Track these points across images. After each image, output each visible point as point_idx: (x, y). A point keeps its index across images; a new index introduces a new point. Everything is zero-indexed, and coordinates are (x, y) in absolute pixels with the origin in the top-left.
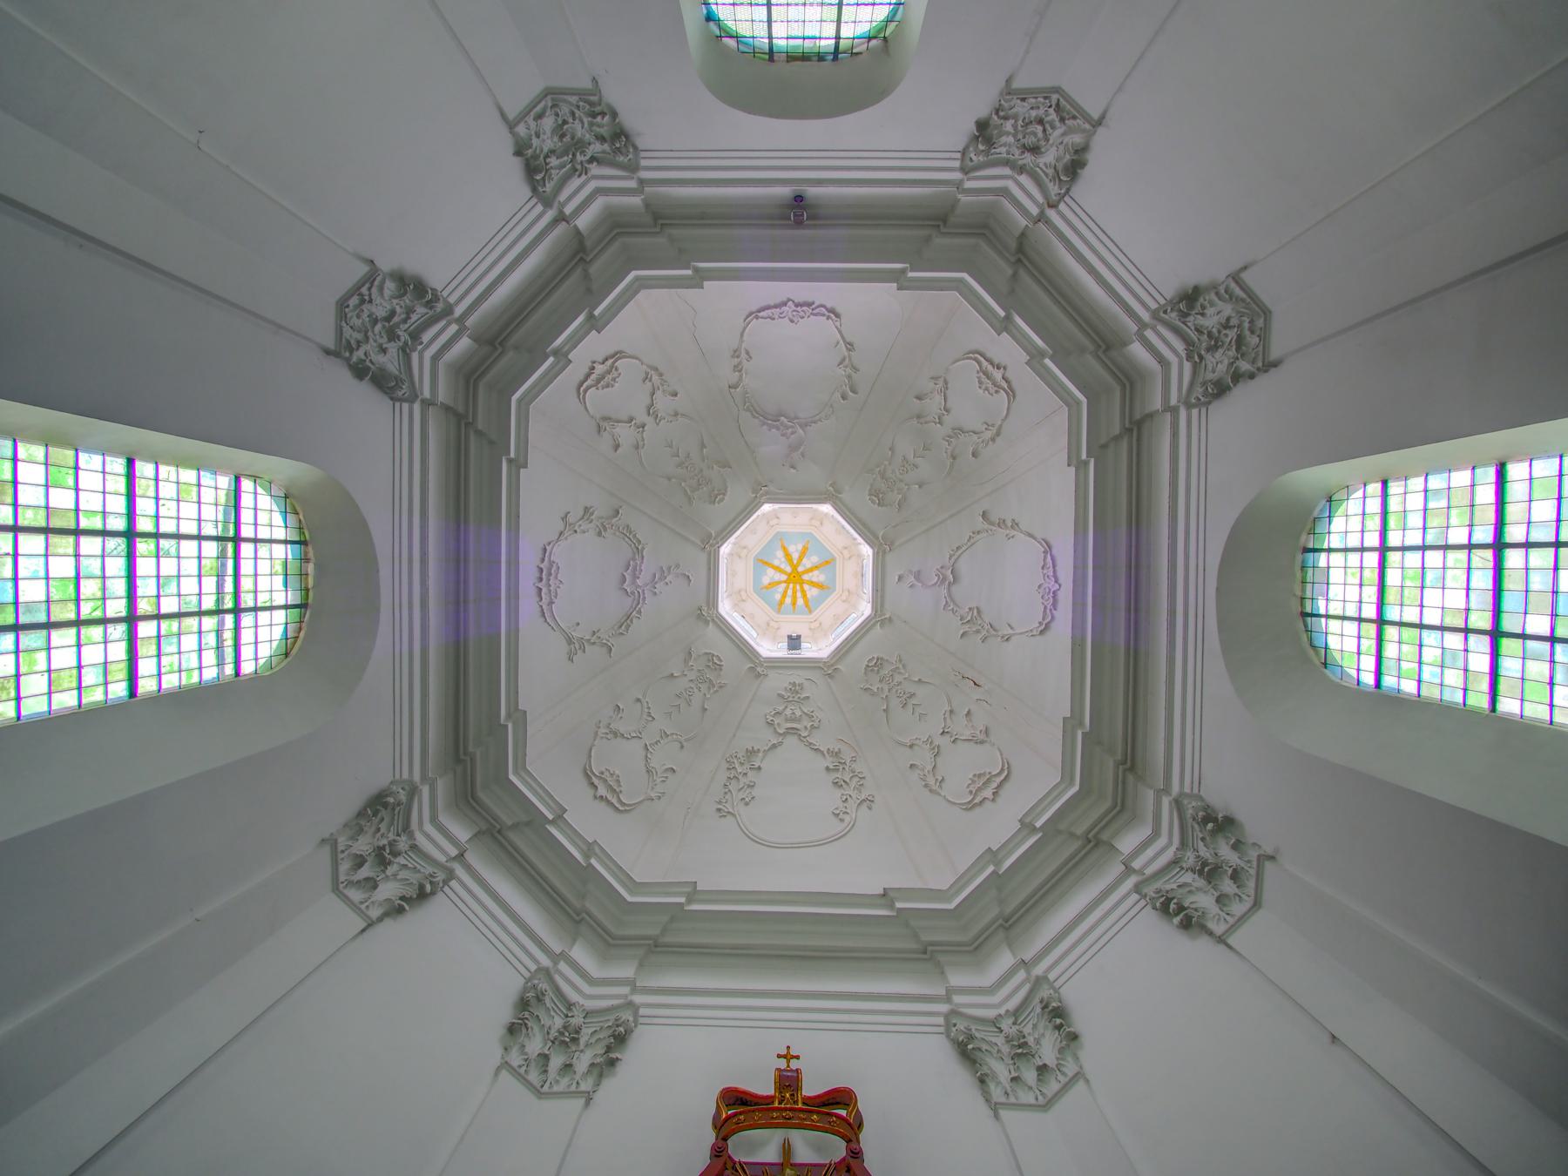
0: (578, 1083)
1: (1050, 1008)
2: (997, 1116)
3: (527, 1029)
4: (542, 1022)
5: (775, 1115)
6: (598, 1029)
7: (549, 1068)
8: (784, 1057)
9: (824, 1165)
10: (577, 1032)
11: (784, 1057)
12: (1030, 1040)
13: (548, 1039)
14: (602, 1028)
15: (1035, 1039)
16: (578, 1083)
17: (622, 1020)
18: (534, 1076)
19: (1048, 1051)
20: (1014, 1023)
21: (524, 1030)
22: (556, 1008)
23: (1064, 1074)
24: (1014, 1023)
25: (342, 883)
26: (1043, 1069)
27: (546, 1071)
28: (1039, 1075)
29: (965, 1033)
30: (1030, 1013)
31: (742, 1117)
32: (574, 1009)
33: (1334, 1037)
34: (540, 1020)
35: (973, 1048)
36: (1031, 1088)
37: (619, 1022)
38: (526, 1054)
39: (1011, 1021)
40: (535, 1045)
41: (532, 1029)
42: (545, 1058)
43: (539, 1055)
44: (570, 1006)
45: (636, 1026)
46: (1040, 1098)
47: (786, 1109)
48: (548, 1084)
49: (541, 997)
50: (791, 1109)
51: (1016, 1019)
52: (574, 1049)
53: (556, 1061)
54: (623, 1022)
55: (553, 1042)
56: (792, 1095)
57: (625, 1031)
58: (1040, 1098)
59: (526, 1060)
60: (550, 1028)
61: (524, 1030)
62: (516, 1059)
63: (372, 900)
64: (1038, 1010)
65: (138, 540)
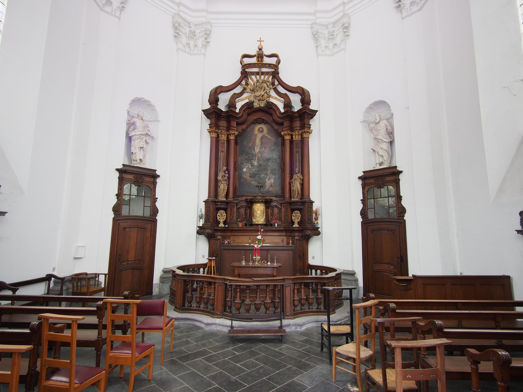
0: (200, 50)
1: (344, 26)
2: (318, 57)
3: (180, 36)
4: (183, 32)
5: (257, 65)
6: (201, 31)
7: (190, 46)
8: (259, 41)
9: (270, 72)
10: (195, 33)
11: (259, 41)
12: (335, 34)
13: (187, 37)
14: (202, 31)
15: (337, 34)
16: (200, 50)
17: (208, 29)
18: (187, 50)
19: (338, 41)
20: (333, 27)
21: (179, 36)
22: (185, 25)
23: (340, 47)
24: (333, 27)
25: (102, 6)
26: (335, 45)
27: (190, 47)
28: (333, 46)
29: (316, 31)
30: (338, 24)
31: (248, 65)
32: (191, 24)
33: (405, 60)
34: (182, 32)
35: (317, 37)
36: (330, 49)
37: (207, 30)
38: (183, 44)
39: (332, 25)
40: (184, 40)
41: (181, 35)
42: (188, 44)
43: (186, 43)
44: (189, 23)
45: (212, 28)
46: (331, 52)
47: (259, 64)
48: (192, 51)
49: (180, 24)
50: (261, 64)
51: (334, 25)
52: (195, 39)
53: (192, 43)
54: (208, 30)
55: (189, 37)
56: (261, 60)
57: (209, 32)
58: (331, 52)
59: (183, 46)
60: (186, 33)
61: (179, 36)
62: (181, 47)
63: (114, 9)
64: (341, 25)
65: (331, 326)
